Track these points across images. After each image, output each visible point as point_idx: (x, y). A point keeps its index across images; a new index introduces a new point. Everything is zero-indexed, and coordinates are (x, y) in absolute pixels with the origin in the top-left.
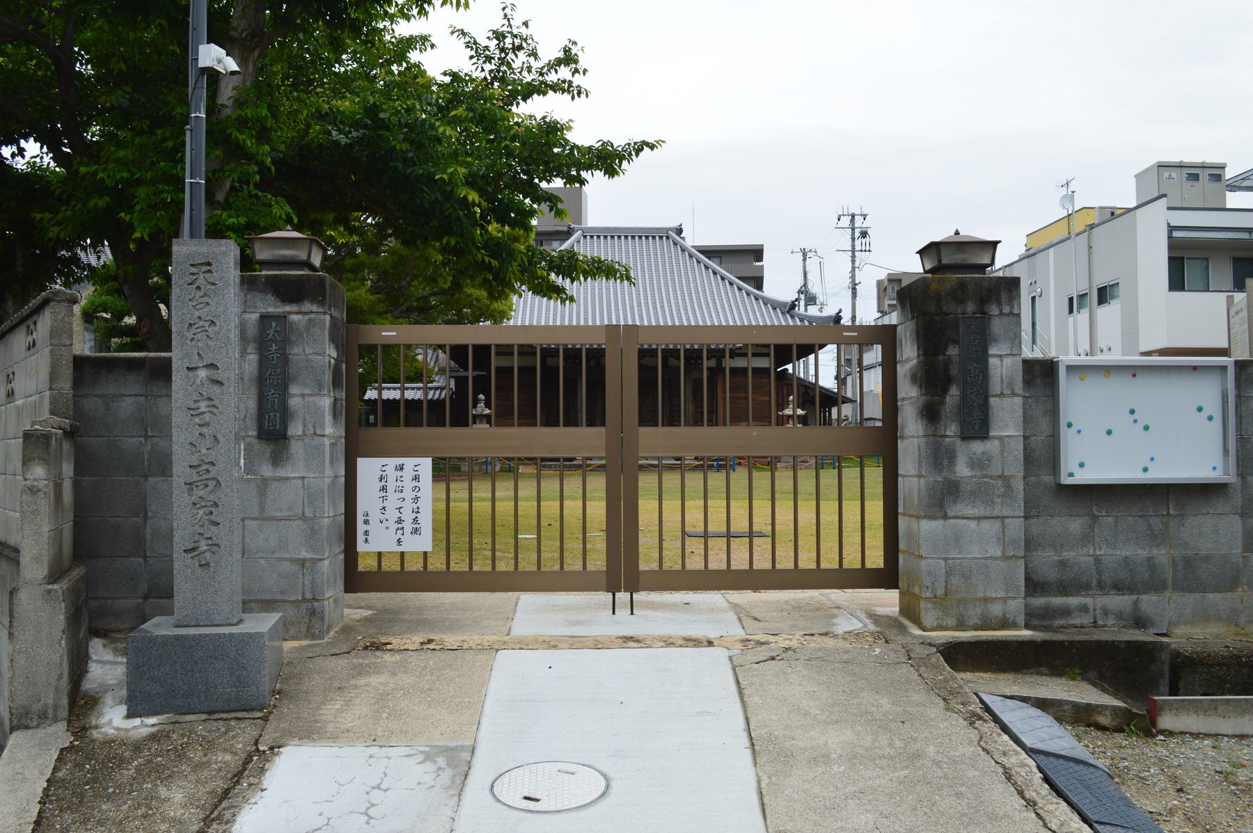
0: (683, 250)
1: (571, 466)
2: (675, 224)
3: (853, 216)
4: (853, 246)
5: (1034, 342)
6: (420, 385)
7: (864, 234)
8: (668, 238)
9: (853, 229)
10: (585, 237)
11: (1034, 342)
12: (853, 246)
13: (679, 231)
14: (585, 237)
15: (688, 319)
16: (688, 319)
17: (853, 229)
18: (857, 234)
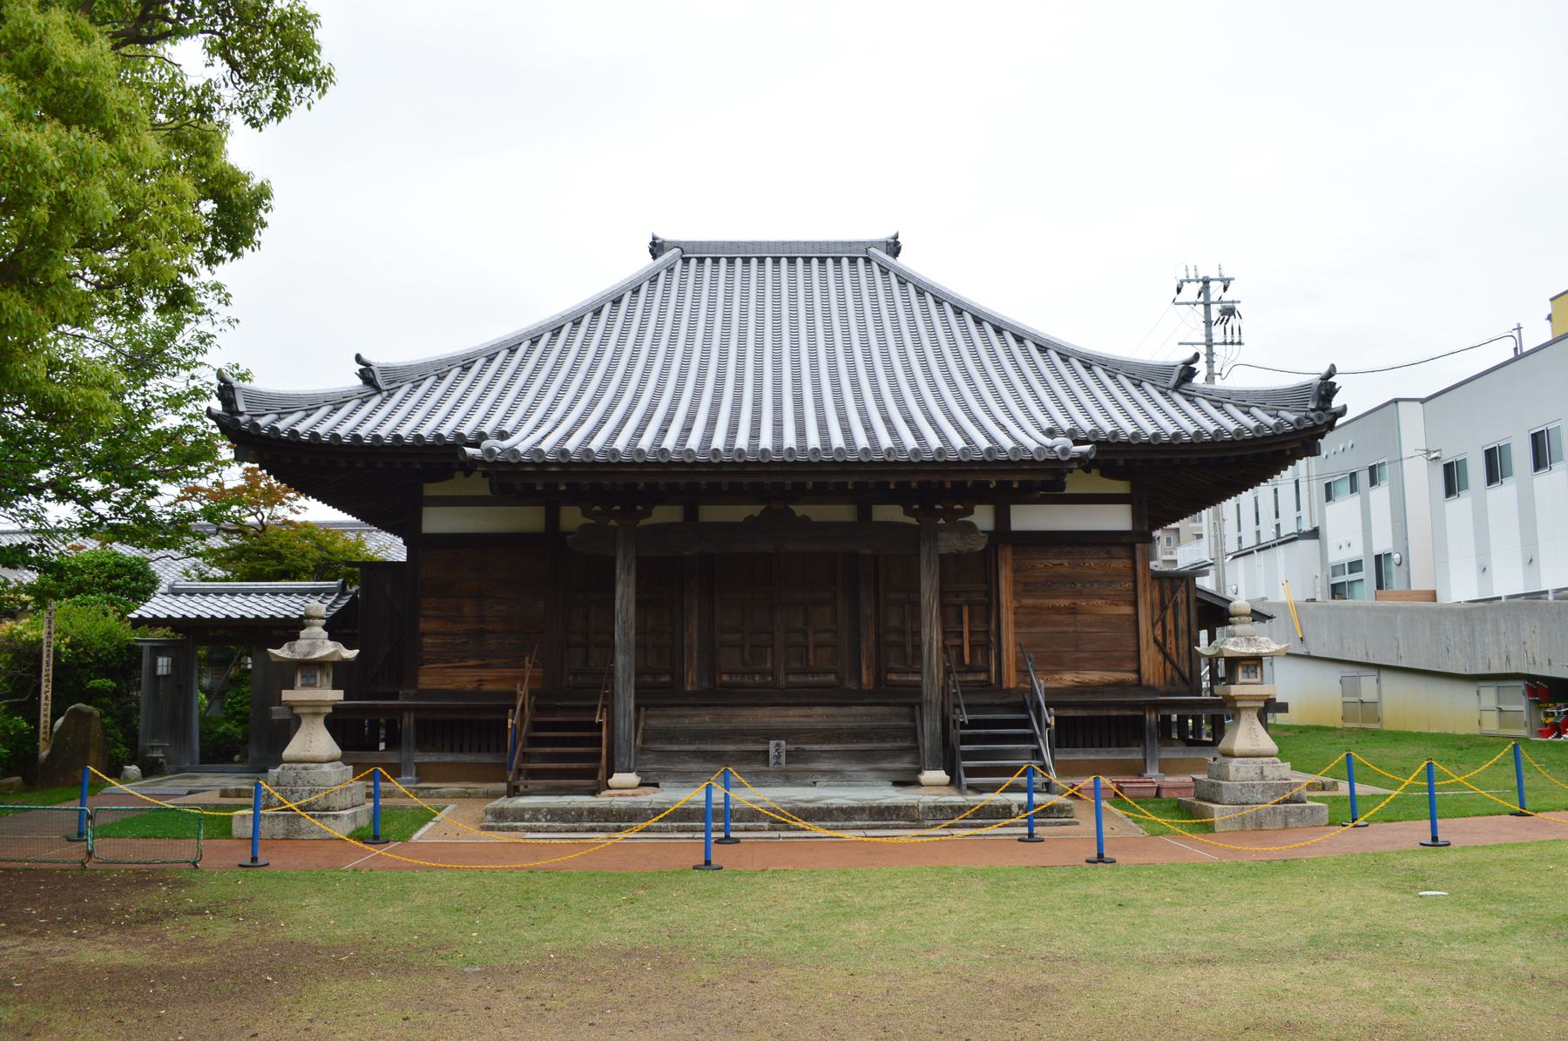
0: (903, 282)
1: (593, 813)
2: (885, 234)
3: (1206, 282)
4: (1209, 335)
5: (1297, 482)
6: (334, 584)
7: (1229, 312)
8: (868, 261)
9: (1207, 305)
10: (686, 261)
11: (1297, 482)
12: (1209, 335)
13: (894, 248)
14: (686, 261)
15: (847, 431)
16: (847, 431)
17: (1207, 305)
18: (1215, 315)
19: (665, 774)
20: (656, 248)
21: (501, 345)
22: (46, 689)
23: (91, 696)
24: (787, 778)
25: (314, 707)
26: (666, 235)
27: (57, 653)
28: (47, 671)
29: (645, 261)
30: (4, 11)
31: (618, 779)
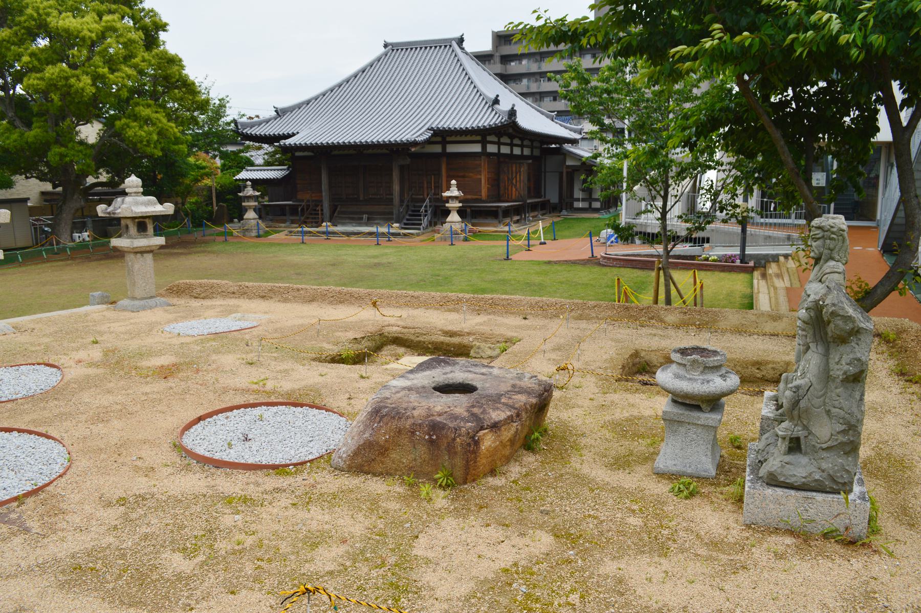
2: (458, 35)
13: (460, 41)
19: (339, 223)
20: (386, 46)
21: (344, 81)
22: (214, 199)
23: (225, 201)
24: (367, 225)
25: (250, 207)
26: (389, 41)
27: (216, 189)
28: (214, 194)
29: (383, 50)
30: (11, 607)
31: (324, 224)
